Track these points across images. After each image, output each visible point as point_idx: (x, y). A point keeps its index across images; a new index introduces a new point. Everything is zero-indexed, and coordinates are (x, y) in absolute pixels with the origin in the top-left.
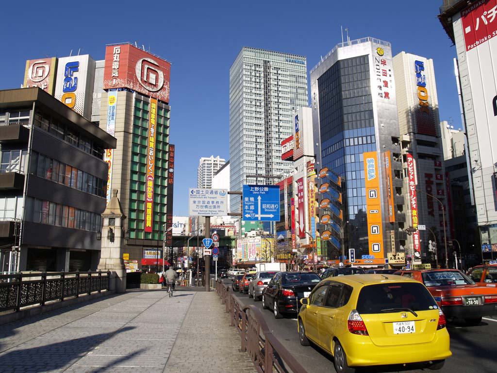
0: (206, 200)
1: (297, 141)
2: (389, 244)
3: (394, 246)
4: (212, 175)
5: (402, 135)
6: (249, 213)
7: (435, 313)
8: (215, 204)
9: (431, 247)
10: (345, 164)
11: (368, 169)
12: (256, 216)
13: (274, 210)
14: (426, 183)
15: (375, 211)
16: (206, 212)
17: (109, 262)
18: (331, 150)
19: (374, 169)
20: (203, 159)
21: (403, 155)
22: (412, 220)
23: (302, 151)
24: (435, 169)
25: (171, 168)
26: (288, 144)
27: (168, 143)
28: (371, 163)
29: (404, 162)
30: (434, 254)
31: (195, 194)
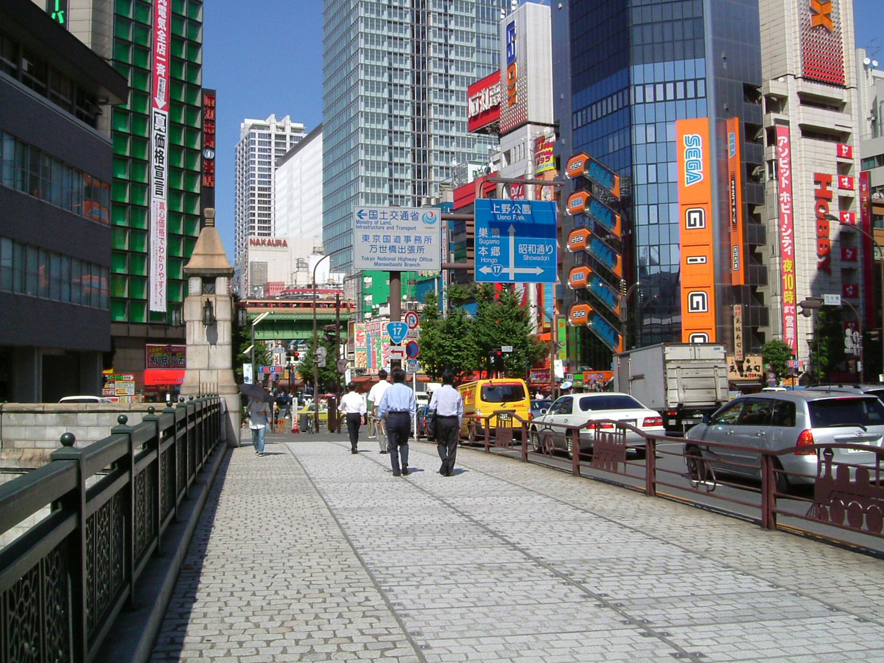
0: (393, 234)
1: (512, 88)
2: (728, 334)
3: (741, 341)
4: (273, 164)
5: (768, 81)
6: (488, 265)
8: (412, 243)
9: (848, 343)
10: (631, 146)
11: (686, 160)
12: (505, 270)
13: (542, 259)
14: (816, 198)
15: (699, 259)
16: (393, 262)
17: (205, 377)
18: (597, 112)
19: (700, 159)
20: (249, 122)
21: (767, 129)
22: (782, 281)
23: (524, 111)
24: (839, 163)
25: (207, 147)
26: (485, 94)
27: (200, 87)
28: (694, 146)
29: (769, 144)
30: (857, 359)
31: (366, 218)
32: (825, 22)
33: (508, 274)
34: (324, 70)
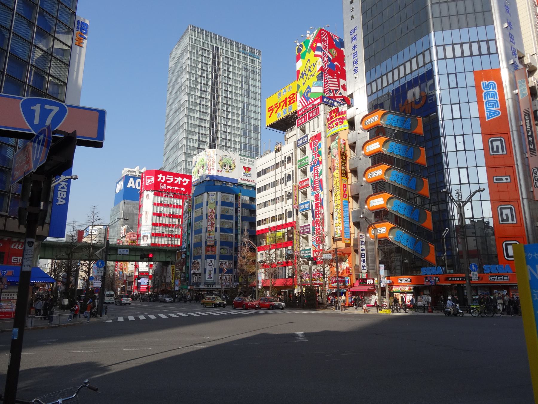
11: (485, 101)
15: (504, 178)
28: (491, 90)
33: (35, 110)
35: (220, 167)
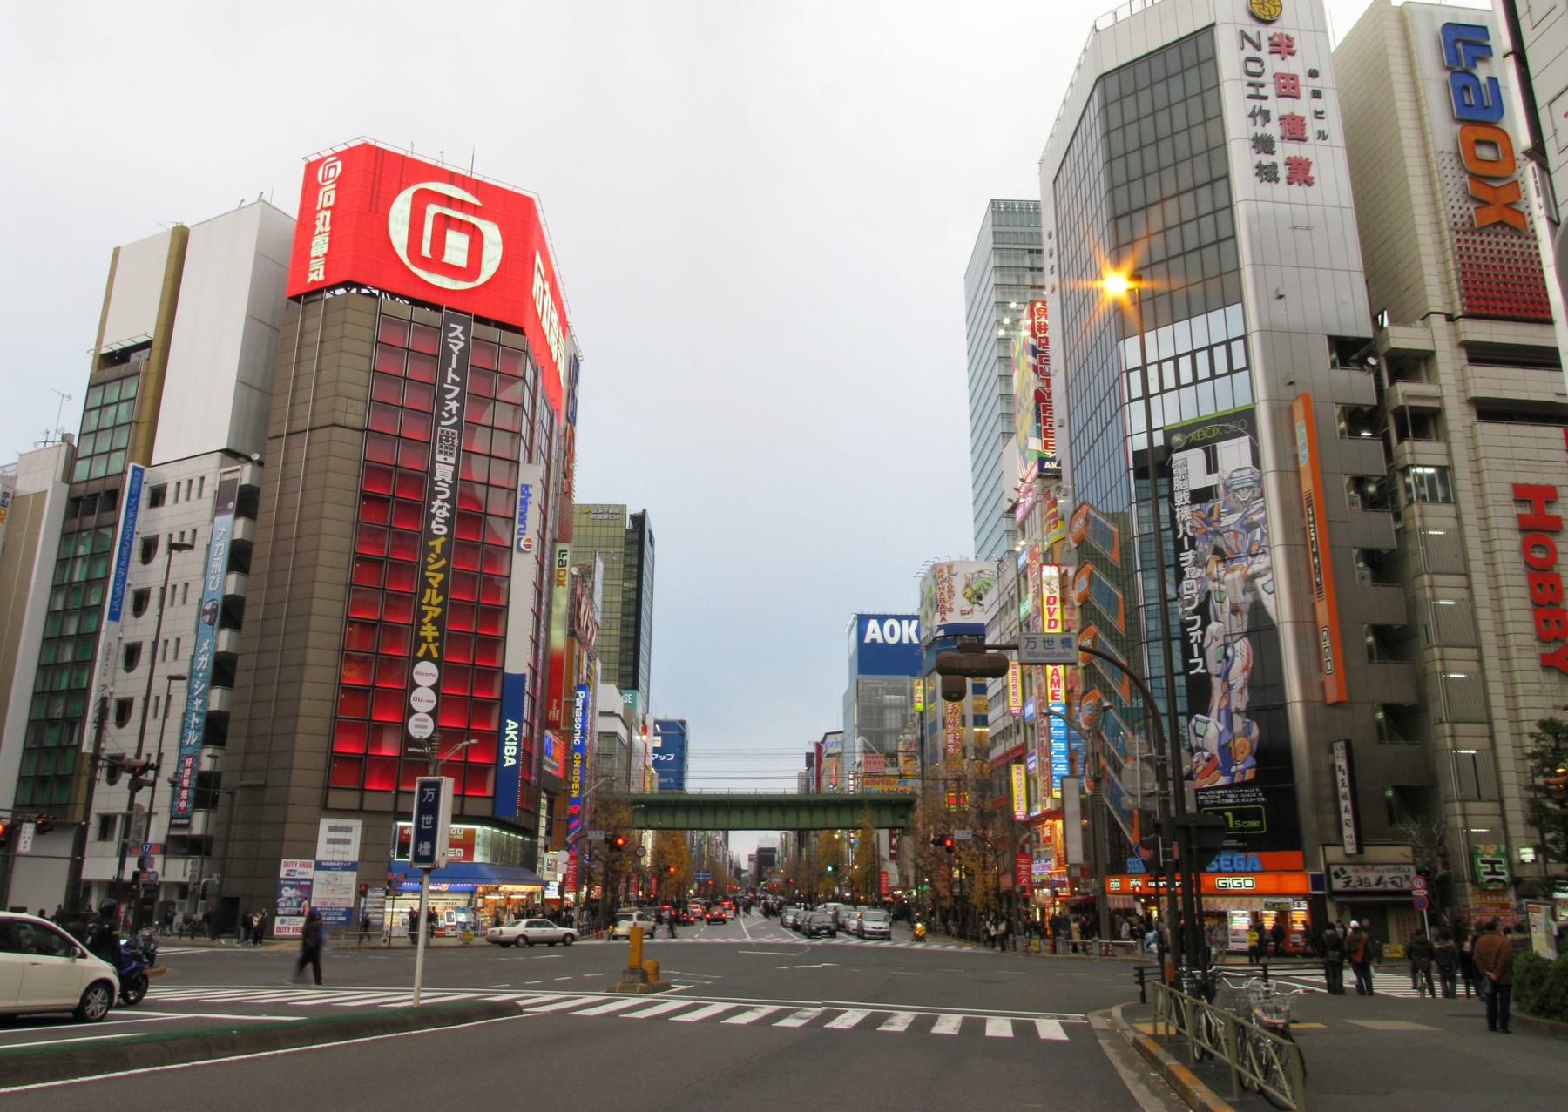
7: (138, 870)
32: (1508, 218)
34: (976, 538)
35: (966, 601)
